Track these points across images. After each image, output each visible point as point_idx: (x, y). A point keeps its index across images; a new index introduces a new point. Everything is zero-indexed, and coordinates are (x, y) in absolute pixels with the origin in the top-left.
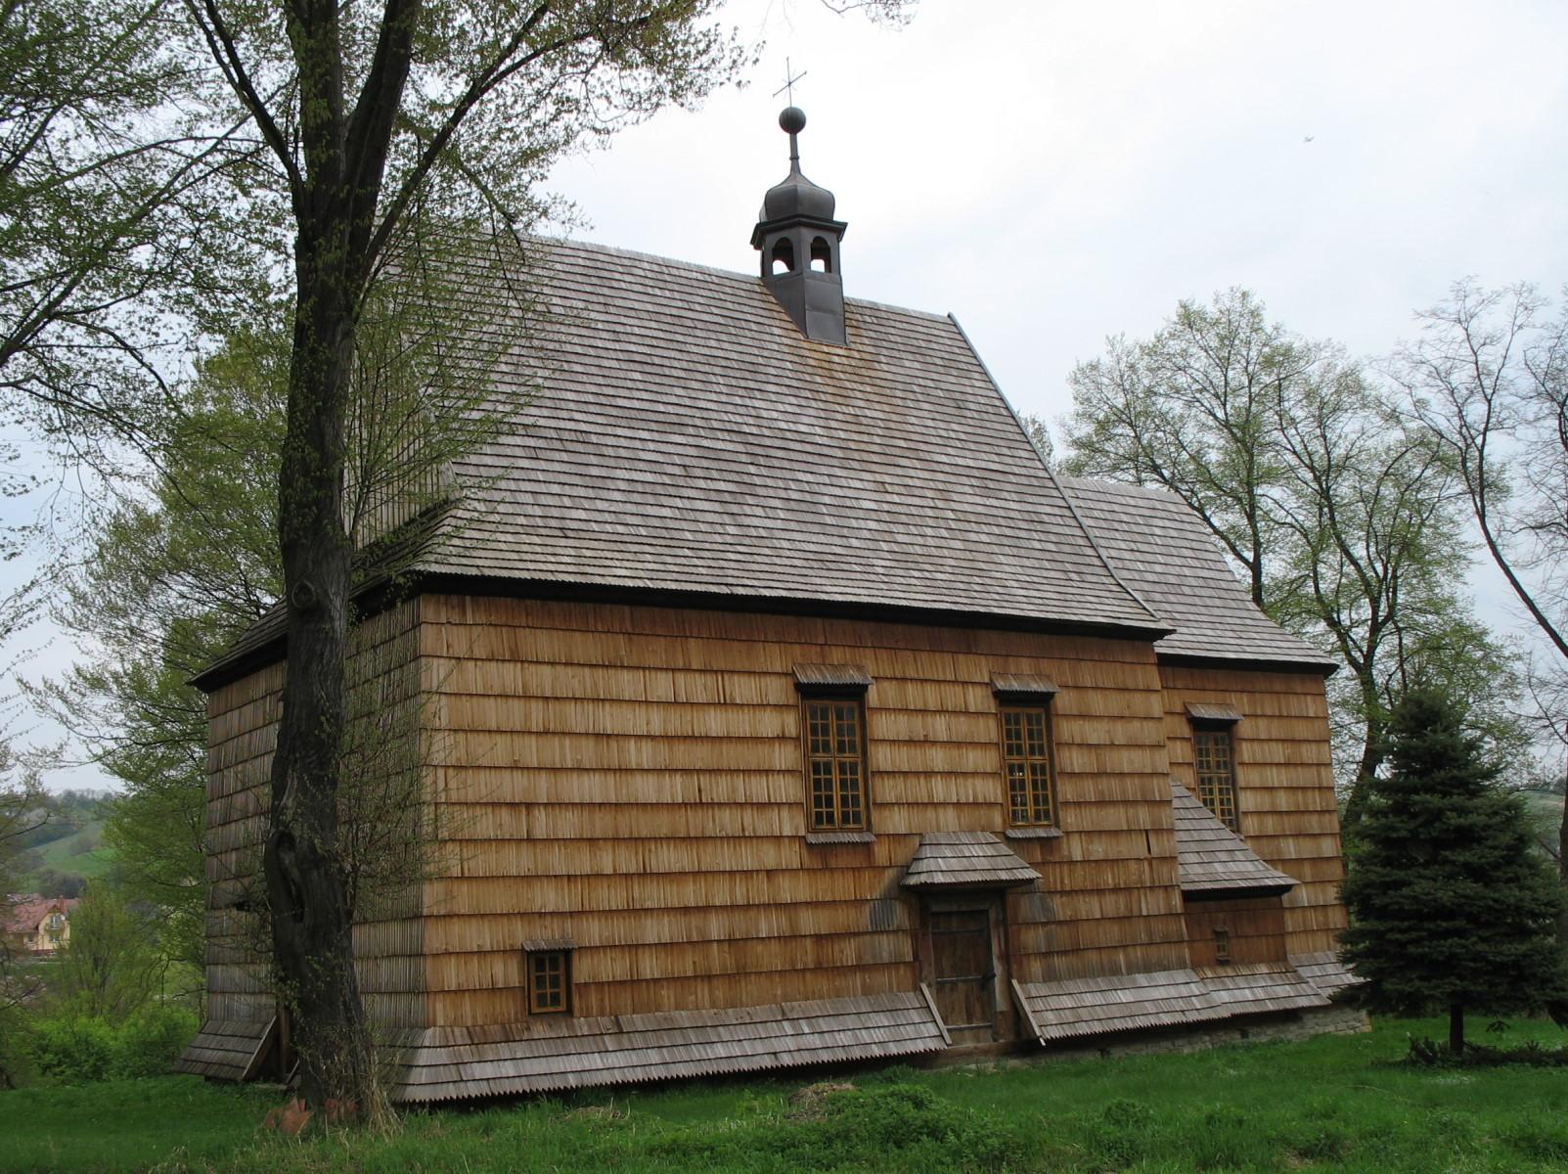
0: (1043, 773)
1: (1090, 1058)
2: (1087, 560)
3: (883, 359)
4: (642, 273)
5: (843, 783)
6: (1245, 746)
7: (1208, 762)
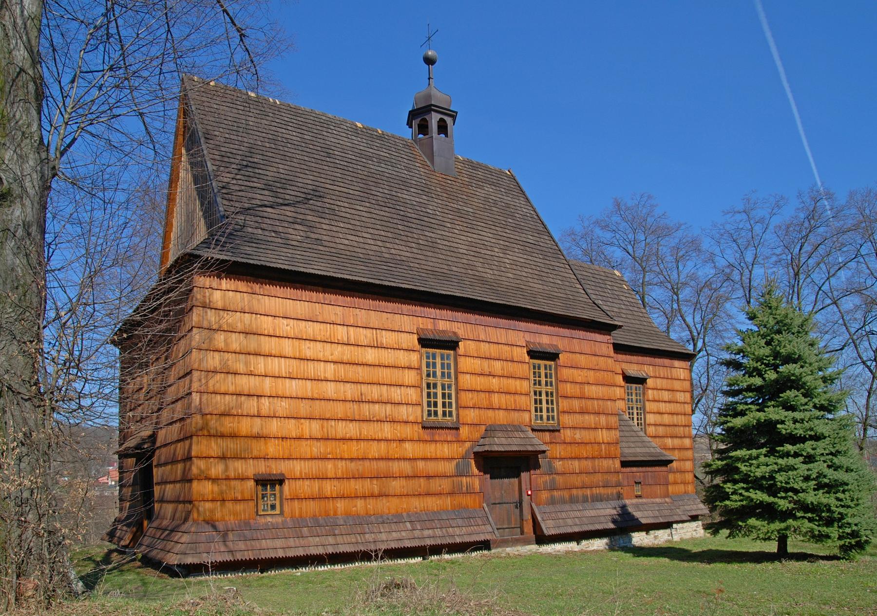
0: (552, 396)
1: (606, 383)
2: (577, 290)
3: (474, 185)
4: (345, 128)
5: (444, 395)
6: (650, 392)
7: (632, 399)
